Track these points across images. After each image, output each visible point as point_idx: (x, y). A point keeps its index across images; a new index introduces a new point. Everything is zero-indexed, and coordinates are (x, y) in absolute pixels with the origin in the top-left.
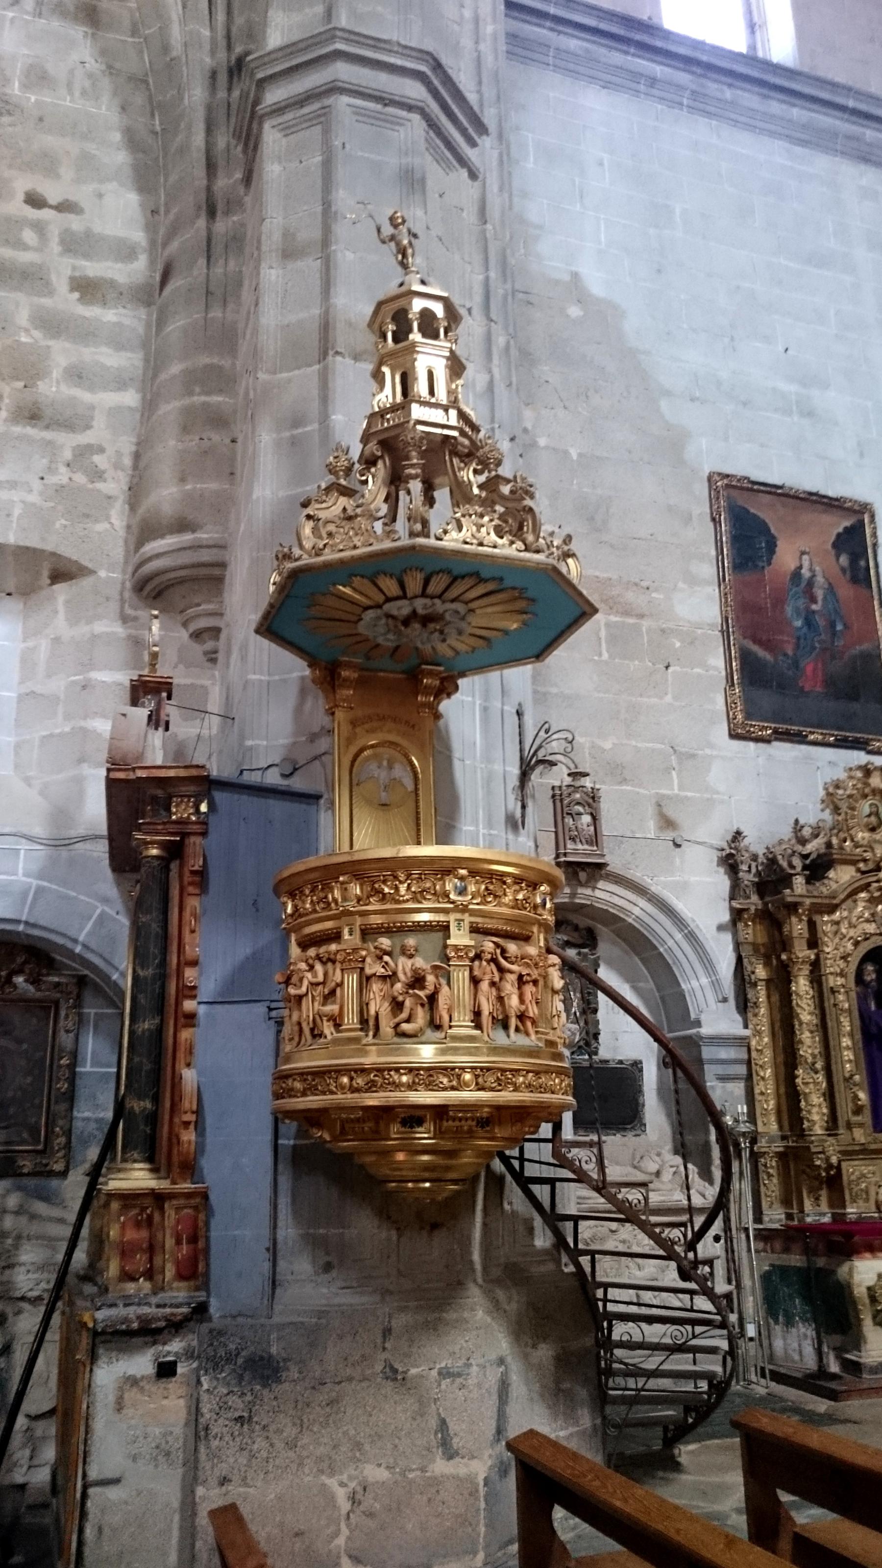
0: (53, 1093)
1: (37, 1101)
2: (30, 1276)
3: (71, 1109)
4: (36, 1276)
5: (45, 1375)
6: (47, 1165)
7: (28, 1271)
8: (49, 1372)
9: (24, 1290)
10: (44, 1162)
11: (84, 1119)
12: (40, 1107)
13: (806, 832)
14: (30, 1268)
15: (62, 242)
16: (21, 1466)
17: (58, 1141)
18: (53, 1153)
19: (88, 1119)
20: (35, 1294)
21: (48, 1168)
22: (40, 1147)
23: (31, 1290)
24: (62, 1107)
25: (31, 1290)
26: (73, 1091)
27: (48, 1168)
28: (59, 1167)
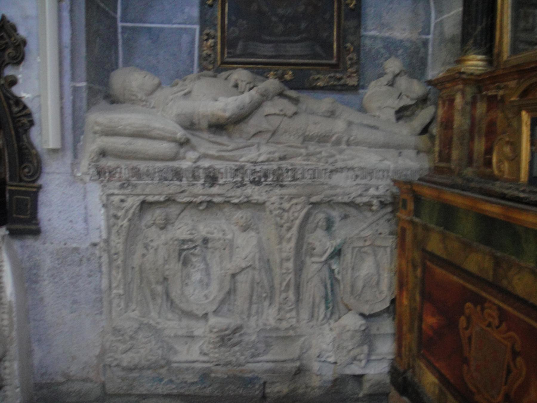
0: (343, 8)
1: (327, 16)
2: (358, 181)
3: (358, 26)
4: (363, 182)
5: (375, 278)
6: (340, 79)
7: (357, 176)
8: (379, 274)
9: (353, 195)
10: (338, 75)
11: (371, 37)
12: (331, 23)
13: (256, 146)
14: (359, 173)
15: (212, 185)
16: (360, 361)
17: (350, 56)
18: (346, 69)
19: (375, 38)
20: (365, 199)
21: (342, 82)
22: (334, 61)
23: (360, 195)
24: (352, 23)
25: (360, 195)
26: (360, 8)
27: (342, 82)
28: (352, 82)
